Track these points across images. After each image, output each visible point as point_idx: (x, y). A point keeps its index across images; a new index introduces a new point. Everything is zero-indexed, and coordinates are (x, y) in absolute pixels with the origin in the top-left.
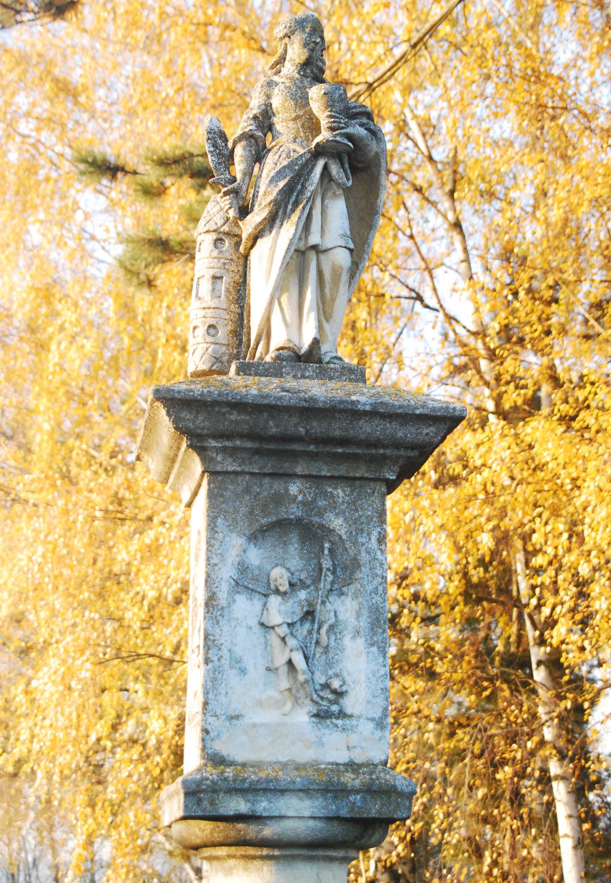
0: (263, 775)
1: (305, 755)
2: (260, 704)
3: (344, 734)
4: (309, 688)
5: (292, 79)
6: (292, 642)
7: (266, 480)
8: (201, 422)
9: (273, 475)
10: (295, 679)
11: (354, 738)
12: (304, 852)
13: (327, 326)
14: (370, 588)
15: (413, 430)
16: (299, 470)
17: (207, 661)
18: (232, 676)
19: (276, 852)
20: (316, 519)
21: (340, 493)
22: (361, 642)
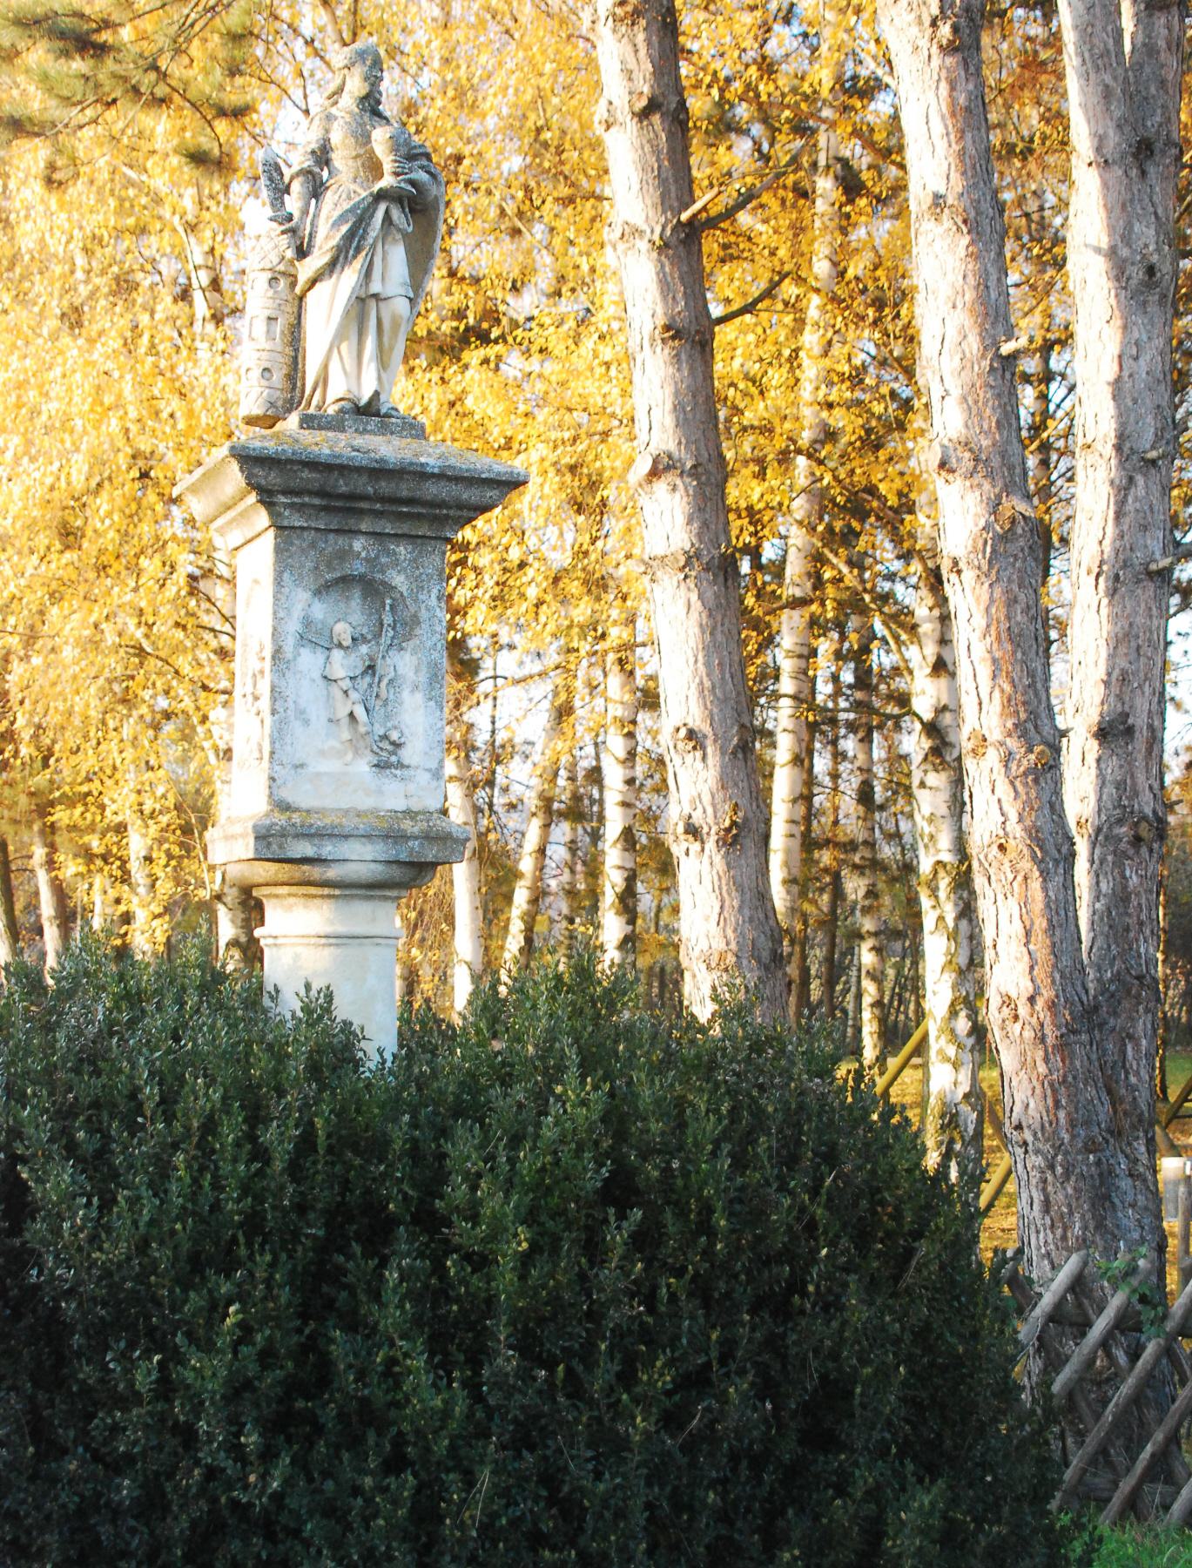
0: (328, 821)
1: (366, 803)
2: (322, 753)
3: (402, 784)
4: (369, 740)
5: (350, 113)
6: (354, 695)
7: (331, 536)
8: (273, 478)
9: (337, 531)
10: (356, 730)
11: (412, 787)
12: (362, 892)
13: (384, 375)
14: (429, 644)
15: (477, 492)
16: (364, 527)
17: (274, 712)
18: (296, 726)
19: (337, 892)
20: (378, 576)
21: (402, 550)
22: (419, 697)
